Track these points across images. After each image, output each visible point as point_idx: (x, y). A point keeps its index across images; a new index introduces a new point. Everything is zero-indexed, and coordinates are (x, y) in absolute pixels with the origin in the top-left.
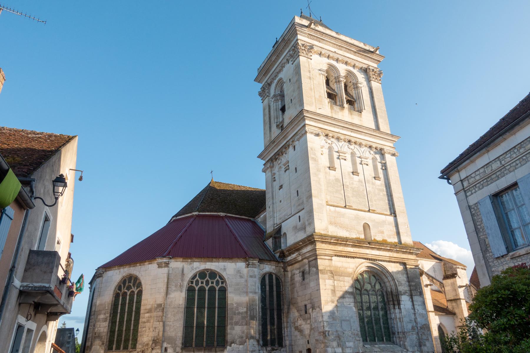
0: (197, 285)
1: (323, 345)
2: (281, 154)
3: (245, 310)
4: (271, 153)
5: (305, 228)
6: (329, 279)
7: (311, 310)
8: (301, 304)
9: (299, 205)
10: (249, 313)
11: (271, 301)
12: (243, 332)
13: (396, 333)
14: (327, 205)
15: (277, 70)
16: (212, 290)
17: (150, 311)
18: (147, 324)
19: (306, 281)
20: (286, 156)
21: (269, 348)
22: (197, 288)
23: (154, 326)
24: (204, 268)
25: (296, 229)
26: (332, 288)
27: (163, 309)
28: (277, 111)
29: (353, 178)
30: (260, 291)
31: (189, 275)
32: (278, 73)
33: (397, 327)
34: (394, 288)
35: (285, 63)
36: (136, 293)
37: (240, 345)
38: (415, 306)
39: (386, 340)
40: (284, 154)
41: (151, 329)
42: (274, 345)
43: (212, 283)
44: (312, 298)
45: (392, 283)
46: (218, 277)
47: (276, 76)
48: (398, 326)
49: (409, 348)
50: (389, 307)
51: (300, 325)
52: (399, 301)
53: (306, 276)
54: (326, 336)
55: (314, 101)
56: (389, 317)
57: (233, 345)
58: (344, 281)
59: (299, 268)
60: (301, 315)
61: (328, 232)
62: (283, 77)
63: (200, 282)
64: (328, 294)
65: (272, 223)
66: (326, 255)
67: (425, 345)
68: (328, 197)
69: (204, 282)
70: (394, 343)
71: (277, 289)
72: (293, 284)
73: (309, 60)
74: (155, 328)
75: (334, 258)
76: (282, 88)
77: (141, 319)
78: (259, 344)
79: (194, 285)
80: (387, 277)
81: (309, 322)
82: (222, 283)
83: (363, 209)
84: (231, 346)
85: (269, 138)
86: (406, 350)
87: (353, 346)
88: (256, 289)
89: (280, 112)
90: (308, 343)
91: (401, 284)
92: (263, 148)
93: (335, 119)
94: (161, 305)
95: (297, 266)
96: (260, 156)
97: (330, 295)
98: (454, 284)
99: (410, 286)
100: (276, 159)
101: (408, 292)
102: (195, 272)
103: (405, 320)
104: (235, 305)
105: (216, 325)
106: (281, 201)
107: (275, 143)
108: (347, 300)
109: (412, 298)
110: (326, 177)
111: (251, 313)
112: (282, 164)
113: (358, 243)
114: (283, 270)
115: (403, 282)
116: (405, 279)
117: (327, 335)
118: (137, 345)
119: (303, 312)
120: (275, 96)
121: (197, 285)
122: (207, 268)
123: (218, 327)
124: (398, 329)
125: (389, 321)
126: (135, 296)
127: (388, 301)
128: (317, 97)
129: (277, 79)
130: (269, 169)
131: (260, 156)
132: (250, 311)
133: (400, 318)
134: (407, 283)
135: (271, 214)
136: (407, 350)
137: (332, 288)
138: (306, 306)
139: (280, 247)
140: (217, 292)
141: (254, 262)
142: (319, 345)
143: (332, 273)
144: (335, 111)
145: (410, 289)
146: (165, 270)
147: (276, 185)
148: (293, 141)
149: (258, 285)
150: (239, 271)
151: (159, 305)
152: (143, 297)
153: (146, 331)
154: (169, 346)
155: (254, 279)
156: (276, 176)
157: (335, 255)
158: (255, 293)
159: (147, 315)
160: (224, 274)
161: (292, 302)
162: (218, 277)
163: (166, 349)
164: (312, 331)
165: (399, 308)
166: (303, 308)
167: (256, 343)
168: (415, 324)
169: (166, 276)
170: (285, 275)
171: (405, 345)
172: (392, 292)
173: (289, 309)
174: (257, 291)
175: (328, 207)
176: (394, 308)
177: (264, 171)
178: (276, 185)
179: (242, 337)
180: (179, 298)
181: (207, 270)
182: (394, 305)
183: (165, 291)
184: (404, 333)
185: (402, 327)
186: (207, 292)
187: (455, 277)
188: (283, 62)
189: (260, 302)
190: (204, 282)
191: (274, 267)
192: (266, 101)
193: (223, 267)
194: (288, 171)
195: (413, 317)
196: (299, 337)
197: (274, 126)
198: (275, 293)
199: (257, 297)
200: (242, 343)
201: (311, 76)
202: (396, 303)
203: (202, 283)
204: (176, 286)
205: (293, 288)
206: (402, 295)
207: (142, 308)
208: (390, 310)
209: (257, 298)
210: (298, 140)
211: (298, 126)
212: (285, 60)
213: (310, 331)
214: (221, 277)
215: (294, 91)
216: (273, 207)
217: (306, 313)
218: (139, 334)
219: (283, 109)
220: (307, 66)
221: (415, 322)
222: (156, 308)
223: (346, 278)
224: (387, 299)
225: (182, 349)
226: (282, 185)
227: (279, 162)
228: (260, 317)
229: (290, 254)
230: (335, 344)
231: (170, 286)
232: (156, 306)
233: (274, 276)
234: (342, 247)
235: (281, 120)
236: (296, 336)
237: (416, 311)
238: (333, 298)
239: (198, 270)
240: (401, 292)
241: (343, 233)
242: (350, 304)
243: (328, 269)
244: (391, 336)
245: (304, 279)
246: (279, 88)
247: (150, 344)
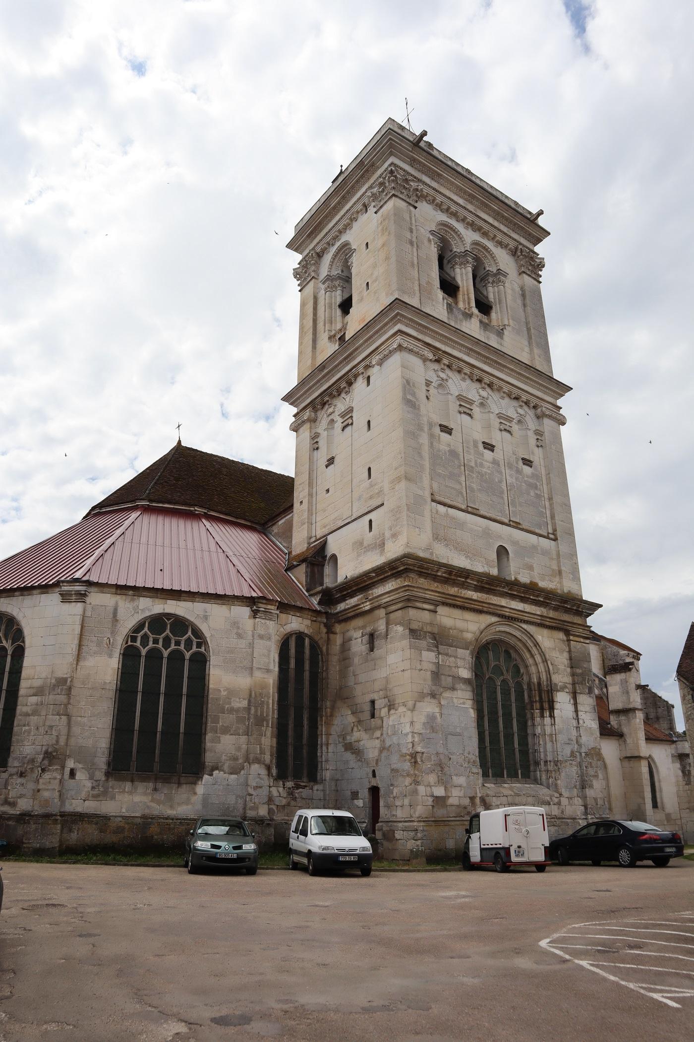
0: (145, 643)
1: (408, 781)
2: (335, 393)
3: (245, 703)
4: (313, 392)
5: (382, 545)
6: (428, 650)
7: (384, 712)
8: (363, 700)
9: (371, 498)
10: (253, 712)
11: (299, 689)
12: (239, 749)
13: (542, 763)
14: (433, 500)
15: (340, 226)
16: (176, 657)
17: (39, 692)
18: (34, 719)
19: (377, 652)
20: (348, 398)
21: (290, 784)
22: (144, 652)
23: (48, 723)
24: (161, 611)
25: (360, 546)
26: (434, 669)
27: (70, 689)
28: (330, 307)
29: (482, 455)
30: (277, 669)
31: (128, 622)
32: (340, 232)
33: (545, 751)
34: (544, 677)
35: (358, 212)
36: (10, 652)
37: (231, 774)
38: (580, 713)
39: (524, 776)
40: (343, 395)
41: (42, 730)
42: (300, 778)
43: (178, 643)
44: (390, 686)
45: (541, 667)
46: (190, 633)
47: (336, 238)
48: (546, 749)
49: (563, 791)
50: (532, 714)
51: (359, 741)
52: (553, 701)
53: (376, 643)
54: (416, 762)
55: (417, 288)
56: (529, 731)
57: (216, 773)
58: (456, 657)
59: (364, 627)
60: (360, 721)
61: (432, 554)
62: (351, 241)
63: (151, 640)
64: (425, 680)
65: (305, 534)
66: (426, 601)
67: (591, 786)
68: (435, 486)
69: (161, 641)
70: (536, 781)
71: (311, 667)
72: (345, 659)
73: (412, 208)
74: (51, 727)
75: (441, 610)
76: (346, 261)
77: (19, 708)
78: (269, 774)
79: (138, 644)
80: (532, 656)
81: (378, 734)
82: (199, 645)
83: (498, 518)
84: (211, 775)
85: (309, 362)
86: (557, 795)
87: (465, 785)
88: (269, 663)
89: (339, 312)
90: (374, 775)
91: (558, 669)
92: (295, 383)
93: (457, 331)
94: (65, 680)
95: (359, 622)
96: (289, 398)
97: (430, 682)
98: (625, 682)
99: (573, 675)
100: (324, 404)
101: (570, 686)
102: (140, 618)
103: (561, 738)
104: (224, 693)
105: (182, 730)
106: (328, 491)
107: (326, 371)
108: (459, 693)
109: (575, 698)
110: (432, 444)
111: (256, 711)
112: (337, 413)
113: (489, 584)
114: (325, 630)
115: (562, 667)
116: (566, 662)
117: (419, 760)
118: (10, 760)
119: (367, 715)
120: (329, 278)
121: (145, 643)
122: (167, 611)
123: (185, 734)
124: (546, 755)
125: (530, 739)
126: (9, 659)
127: (532, 702)
128: (423, 283)
129: (338, 244)
130: (307, 426)
131: (289, 398)
132: (256, 707)
133: (551, 735)
134: (569, 670)
135: (306, 515)
136: (561, 795)
137: (434, 669)
138: (373, 702)
139: (322, 584)
140: (187, 663)
141: (269, 607)
142: (401, 779)
143: (435, 639)
144: (456, 317)
145: (573, 680)
146: (78, 608)
147: (322, 457)
148: (367, 367)
149: (275, 656)
150: (235, 623)
151: (62, 681)
152: (27, 662)
153: (29, 732)
154: (80, 766)
155: (268, 643)
156: (322, 443)
157: (444, 604)
158: (268, 671)
159: (34, 699)
160: (203, 628)
161: (344, 696)
162: (190, 633)
163: (72, 773)
164: (384, 754)
165: (552, 716)
166: (367, 707)
167: (264, 772)
168: (576, 746)
169: (78, 620)
170: (328, 639)
171: (556, 785)
172: (539, 684)
173: (333, 708)
174: (271, 667)
175: (434, 504)
176: (542, 716)
177: (295, 428)
178: (322, 457)
179: (235, 759)
180: (106, 668)
181: (168, 615)
182: (542, 709)
183: (75, 653)
184: (556, 763)
185: (553, 752)
186: (165, 661)
187: (630, 670)
188: (354, 209)
189: (276, 690)
190: (161, 641)
191: (308, 622)
192: (310, 288)
193: (202, 613)
194: (349, 429)
195: (574, 733)
196: (352, 764)
197: (323, 338)
198: (307, 675)
199: (271, 680)
200: (234, 771)
201: (414, 239)
202: (546, 705)
203: (156, 641)
204: (99, 644)
205: (347, 667)
206: (558, 691)
207: (23, 684)
208: (533, 719)
209: (271, 681)
210: (380, 363)
211: (381, 336)
212: (359, 206)
213: (381, 752)
214: (197, 633)
215: (375, 266)
216: (310, 503)
217: (373, 716)
218: (14, 739)
219: (346, 306)
220: (408, 219)
221: (577, 742)
222: (54, 687)
223: (460, 652)
224: (530, 697)
225: (108, 774)
226: (333, 458)
227: (331, 410)
228: (275, 721)
229: (343, 599)
230: (432, 778)
231: (85, 642)
232: (53, 681)
233: (307, 641)
234: (456, 589)
235: (339, 326)
236: (347, 762)
237: (581, 722)
238: (434, 688)
239: (148, 614)
240: (556, 684)
241: (460, 561)
242: (464, 703)
243: (429, 629)
244: (532, 768)
245: (372, 649)
246: (340, 264)
247: (39, 760)
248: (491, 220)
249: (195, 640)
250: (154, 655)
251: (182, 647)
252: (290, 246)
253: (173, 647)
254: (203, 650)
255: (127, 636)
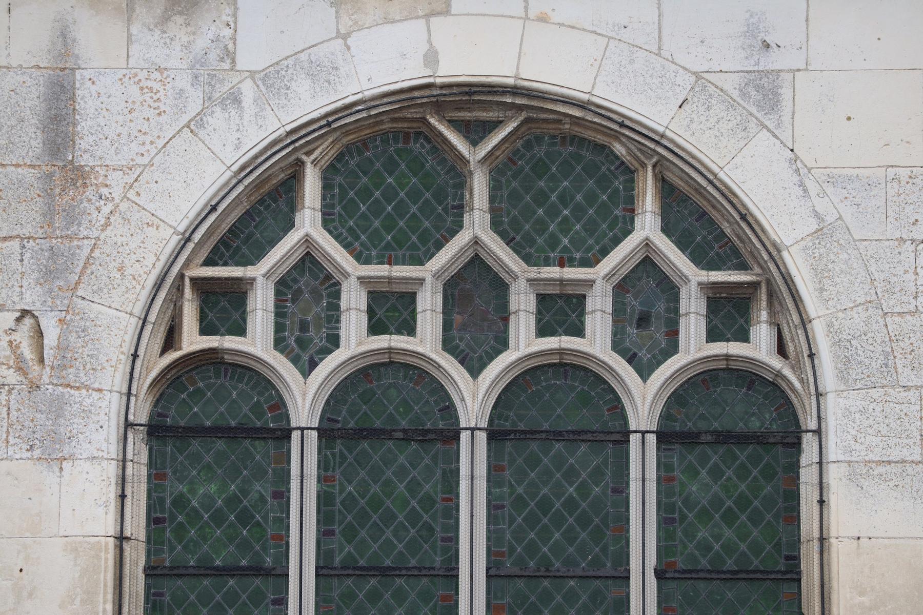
0: (306, 336)
16: (557, 416)
46: (648, 225)
79: (257, 340)
82: (729, 312)
121: (306, 336)
160: (753, 174)
162: (648, 225)
203: (391, 310)
214: (706, 219)
239: (307, 103)
248: (347, 120)
249: (692, 277)
250: (387, 419)
251: (596, 340)
252: (583, 336)
253: (525, 341)
254: (759, 347)
255: (171, 286)
